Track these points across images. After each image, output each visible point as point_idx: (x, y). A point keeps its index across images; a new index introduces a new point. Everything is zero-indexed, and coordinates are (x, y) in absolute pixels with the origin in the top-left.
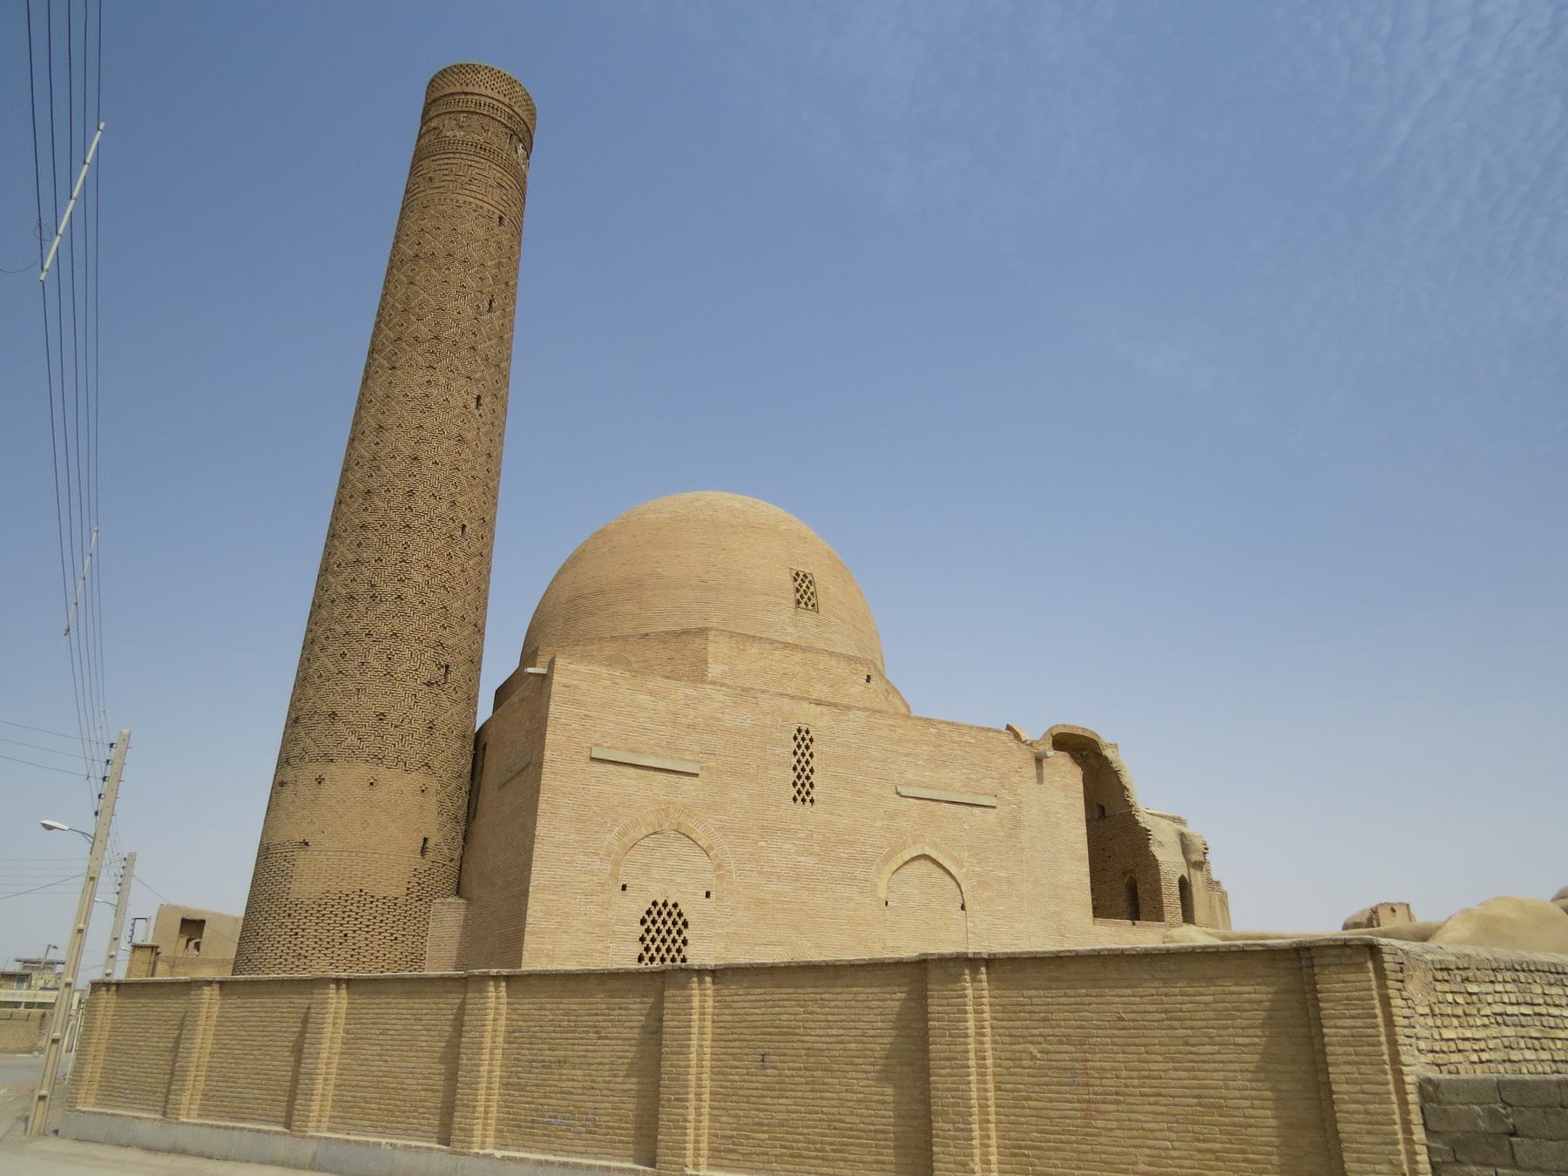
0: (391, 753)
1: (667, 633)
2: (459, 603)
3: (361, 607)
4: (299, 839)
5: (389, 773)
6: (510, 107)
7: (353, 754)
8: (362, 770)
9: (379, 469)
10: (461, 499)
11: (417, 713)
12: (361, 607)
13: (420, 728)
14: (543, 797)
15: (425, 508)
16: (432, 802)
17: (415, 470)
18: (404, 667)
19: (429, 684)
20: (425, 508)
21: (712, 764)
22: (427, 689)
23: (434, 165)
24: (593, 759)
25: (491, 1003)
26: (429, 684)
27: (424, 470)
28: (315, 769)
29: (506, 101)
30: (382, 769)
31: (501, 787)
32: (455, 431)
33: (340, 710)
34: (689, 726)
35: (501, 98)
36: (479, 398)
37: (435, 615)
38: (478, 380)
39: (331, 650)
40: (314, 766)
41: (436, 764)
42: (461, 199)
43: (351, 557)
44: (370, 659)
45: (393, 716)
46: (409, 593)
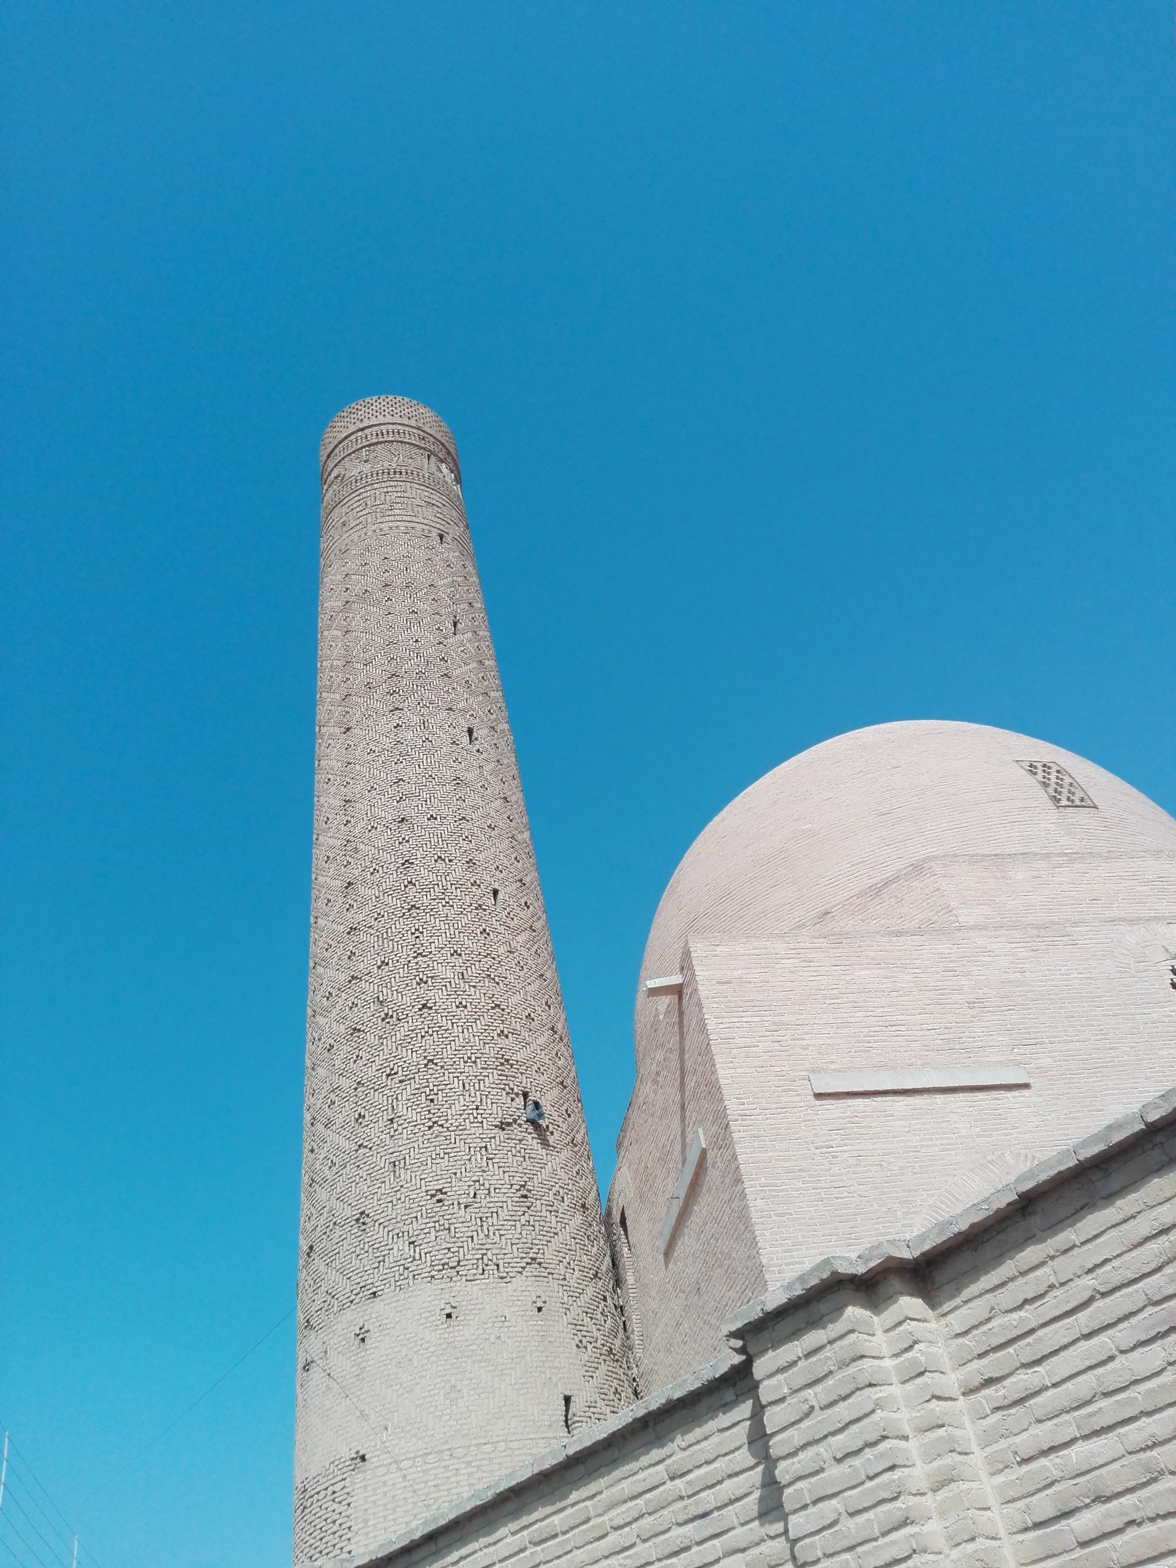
0: (471, 1256)
1: (859, 895)
2: (516, 999)
3: (371, 1039)
4: (347, 1454)
5: (474, 1289)
6: (419, 428)
7: (407, 1272)
8: (427, 1297)
9: (356, 850)
10: (481, 857)
11: (495, 1176)
12: (371, 1039)
13: (508, 1199)
14: (751, 1187)
15: (433, 877)
16: (560, 1327)
17: (406, 834)
18: (458, 1107)
19: (502, 1126)
20: (433, 877)
21: (1046, 1061)
22: (502, 1135)
23: (345, 509)
24: (819, 1096)
25: (899, 1405)
26: (502, 1126)
27: (418, 831)
28: (347, 1322)
29: (413, 422)
30: (459, 1285)
31: (668, 1254)
32: (449, 774)
33: (370, 1206)
34: (971, 1005)
35: (406, 422)
36: (470, 731)
37: (486, 1020)
38: (464, 711)
39: (339, 1121)
40: (348, 1315)
41: (549, 1255)
42: (385, 527)
43: (343, 977)
44: (401, 1109)
45: (458, 1190)
46: (436, 996)
